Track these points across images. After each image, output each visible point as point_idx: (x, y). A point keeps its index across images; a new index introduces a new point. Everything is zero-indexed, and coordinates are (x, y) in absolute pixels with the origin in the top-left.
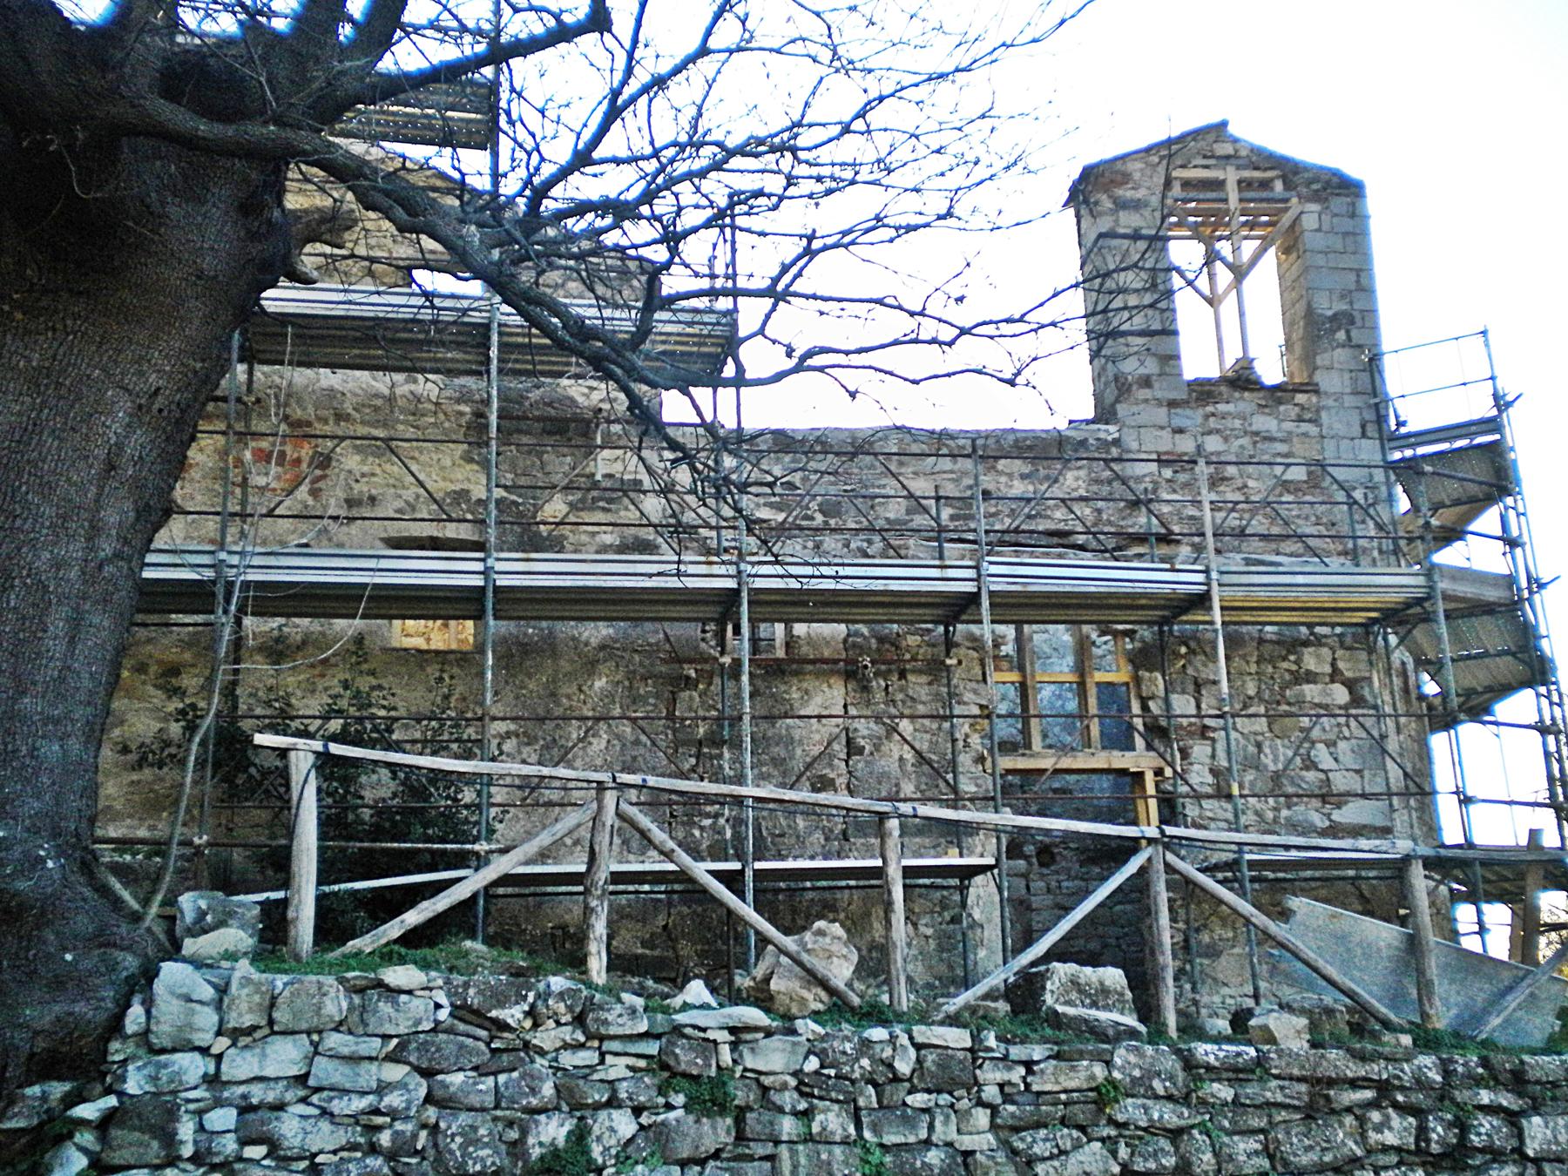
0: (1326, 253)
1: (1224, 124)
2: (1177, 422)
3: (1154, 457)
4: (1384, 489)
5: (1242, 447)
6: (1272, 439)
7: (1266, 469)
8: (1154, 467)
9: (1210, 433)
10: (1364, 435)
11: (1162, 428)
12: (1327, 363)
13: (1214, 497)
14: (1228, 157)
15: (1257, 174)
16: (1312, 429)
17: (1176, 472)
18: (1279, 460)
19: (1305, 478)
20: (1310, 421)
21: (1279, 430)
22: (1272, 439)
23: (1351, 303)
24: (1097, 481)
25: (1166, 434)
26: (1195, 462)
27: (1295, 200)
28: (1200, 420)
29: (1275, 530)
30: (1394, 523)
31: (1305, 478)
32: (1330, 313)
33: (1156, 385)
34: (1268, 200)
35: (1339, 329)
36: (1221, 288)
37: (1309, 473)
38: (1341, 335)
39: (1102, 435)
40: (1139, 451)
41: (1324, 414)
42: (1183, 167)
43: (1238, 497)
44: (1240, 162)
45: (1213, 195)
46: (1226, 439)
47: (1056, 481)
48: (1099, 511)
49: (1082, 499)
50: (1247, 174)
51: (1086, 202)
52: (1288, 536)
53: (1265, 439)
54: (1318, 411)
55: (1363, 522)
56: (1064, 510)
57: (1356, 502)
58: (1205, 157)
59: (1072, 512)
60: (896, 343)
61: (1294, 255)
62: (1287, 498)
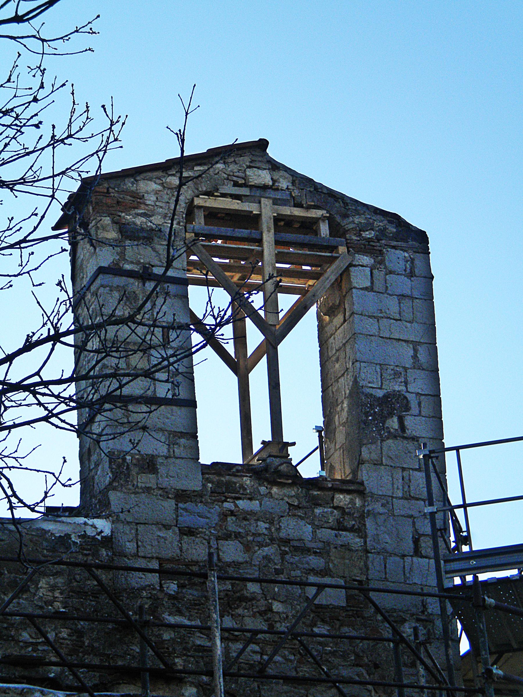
0: (378, 319)
1: (263, 144)
2: (186, 520)
3: (155, 565)
4: (438, 623)
5: (266, 557)
6: (308, 551)
7: (297, 590)
8: (153, 579)
9: (227, 537)
10: (417, 552)
11: (167, 527)
12: (374, 456)
13: (228, 622)
14: (265, 187)
15: (297, 212)
16: (356, 541)
17: (181, 586)
18: (312, 579)
19: (343, 603)
20: (351, 530)
21: (314, 538)
22: (308, 551)
23: (406, 383)
24: (80, 593)
25: (171, 535)
26: (205, 576)
27: (342, 249)
28: (215, 519)
29: (306, 671)
30: (449, 668)
31: (343, 603)
32: (380, 394)
33: (162, 470)
34: (311, 246)
35: (391, 415)
36: (251, 348)
37: (349, 598)
38: (393, 423)
39: (90, 532)
40: (136, 555)
41: (369, 523)
42: (209, 194)
43: (260, 624)
44: (278, 195)
45: (244, 233)
46: (247, 548)
47: (24, 589)
48: (80, 634)
49: (57, 616)
50: (287, 211)
51: (85, 225)
52: (320, 681)
53: (296, 549)
54: (362, 517)
55: (413, 665)
56: (33, 630)
57: (403, 640)
58: (236, 184)
59: (44, 635)
60: (40, 266)
61: (339, 318)
62: (321, 629)
